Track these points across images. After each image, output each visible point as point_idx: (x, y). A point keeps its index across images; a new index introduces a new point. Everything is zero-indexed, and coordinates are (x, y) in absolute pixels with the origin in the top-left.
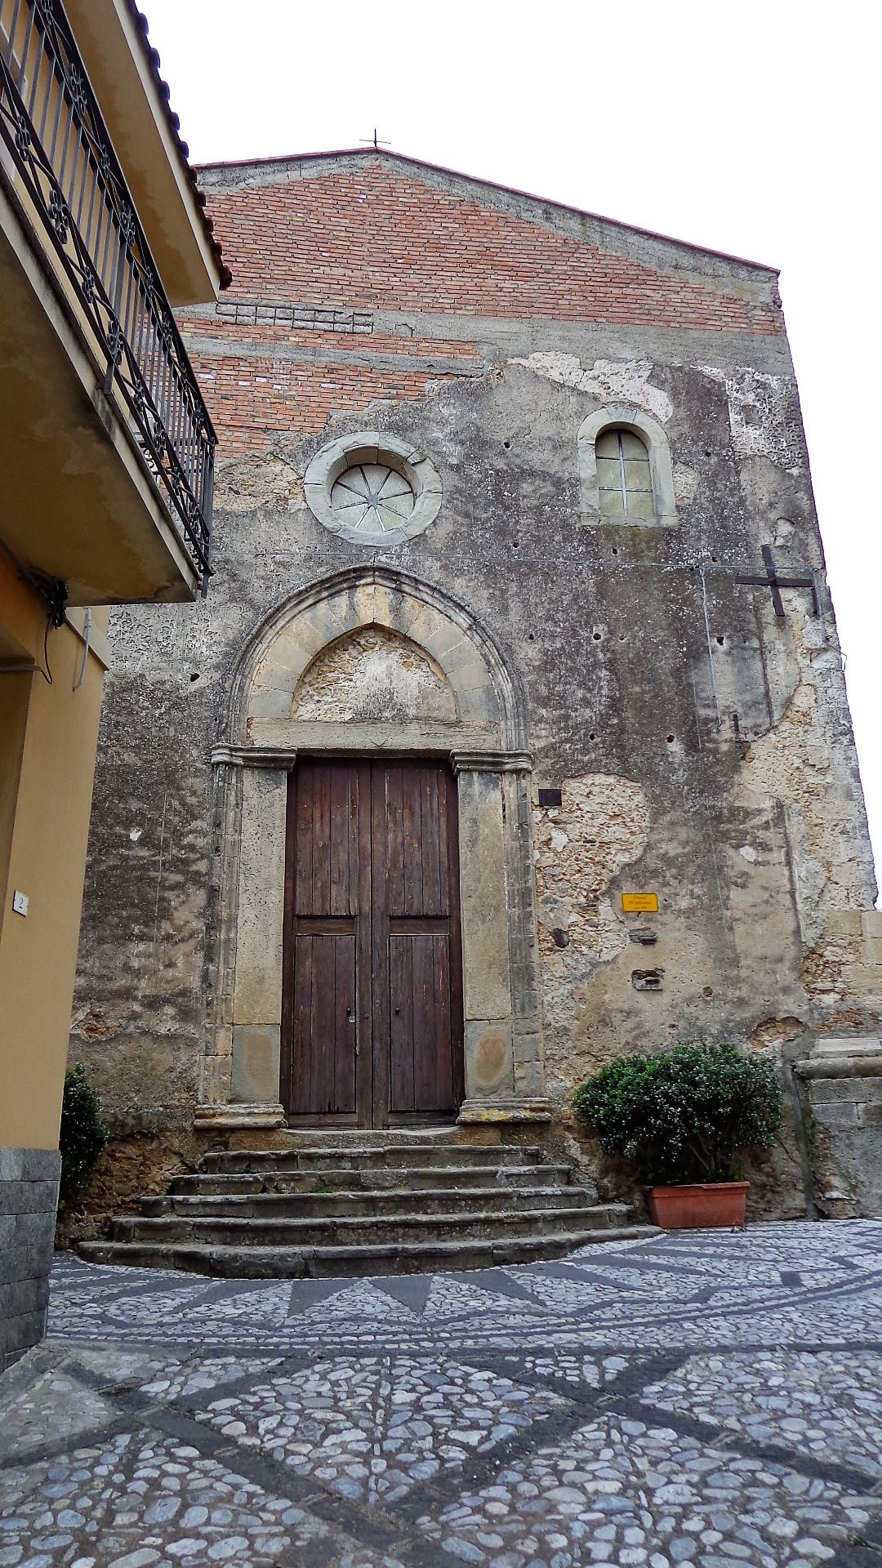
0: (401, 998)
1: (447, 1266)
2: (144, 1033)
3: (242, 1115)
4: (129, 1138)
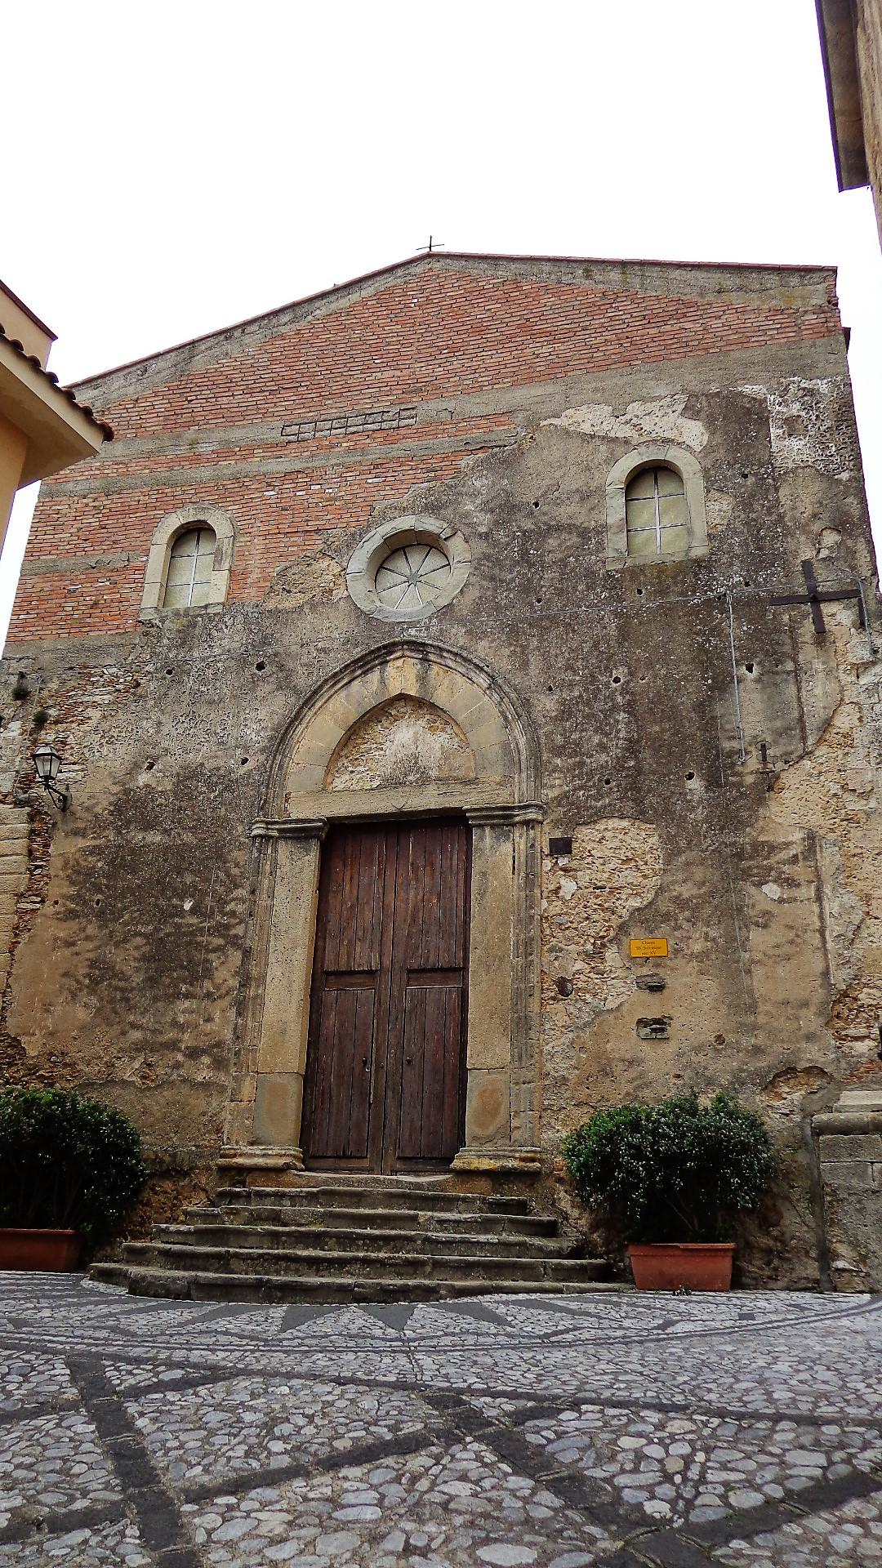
2: (184, 1081)
4: (166, 1174)
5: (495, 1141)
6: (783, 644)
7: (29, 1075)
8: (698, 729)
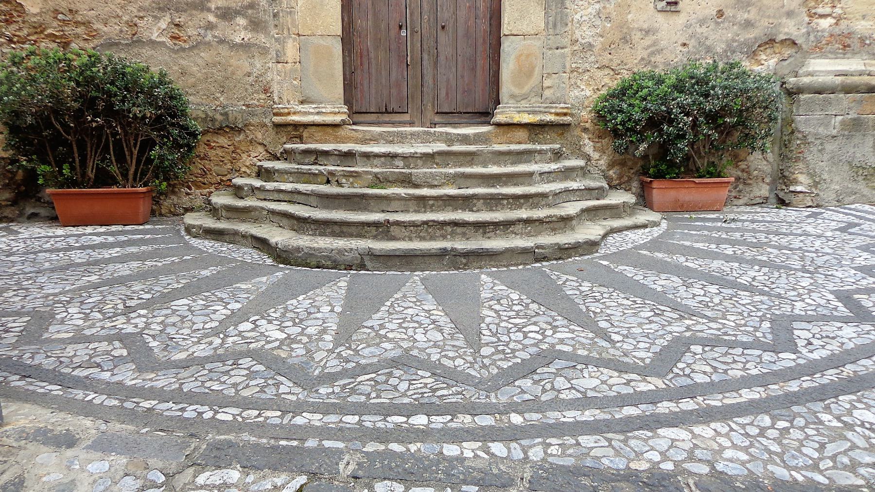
0: (446, 15)
1: (492, 263)
2: (221, 42)
3: (312, 113)
4: (220, 130)
5: (529, 98)
7: (36, 33)
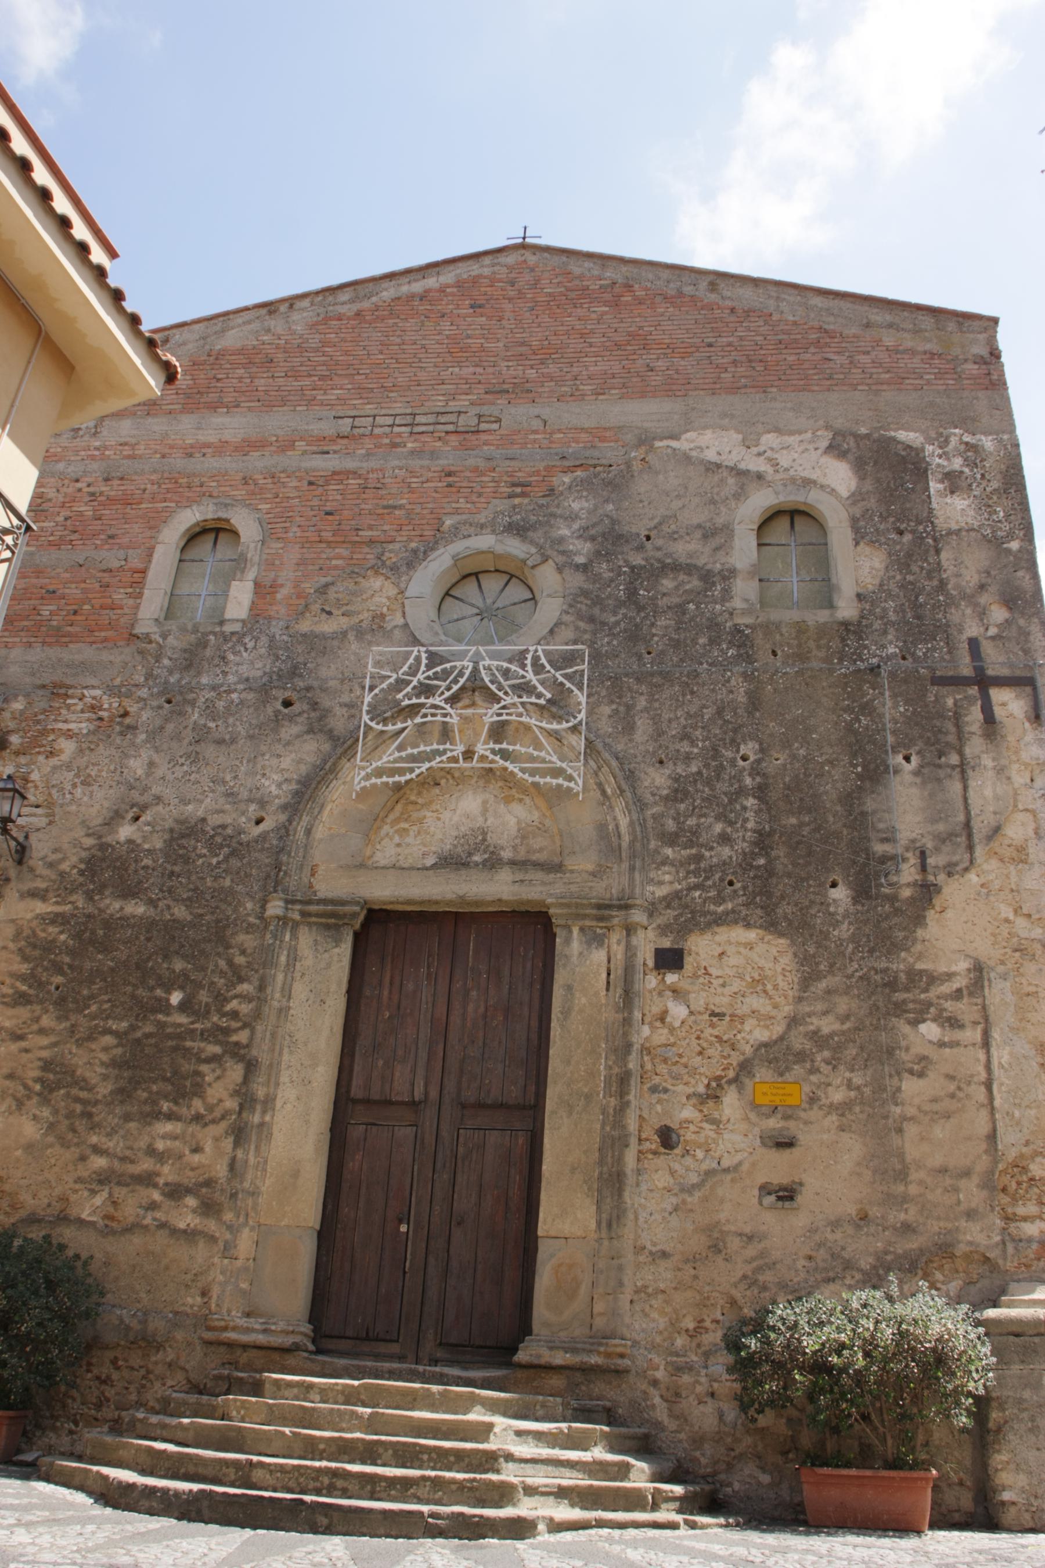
2: (163, 1225)
6: (946, 734)
8: (845, 826)
